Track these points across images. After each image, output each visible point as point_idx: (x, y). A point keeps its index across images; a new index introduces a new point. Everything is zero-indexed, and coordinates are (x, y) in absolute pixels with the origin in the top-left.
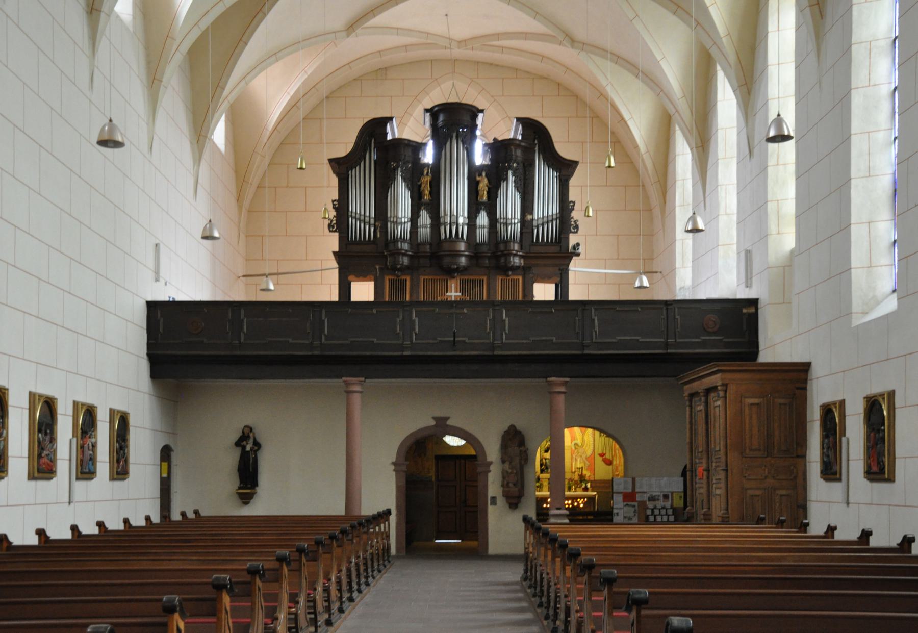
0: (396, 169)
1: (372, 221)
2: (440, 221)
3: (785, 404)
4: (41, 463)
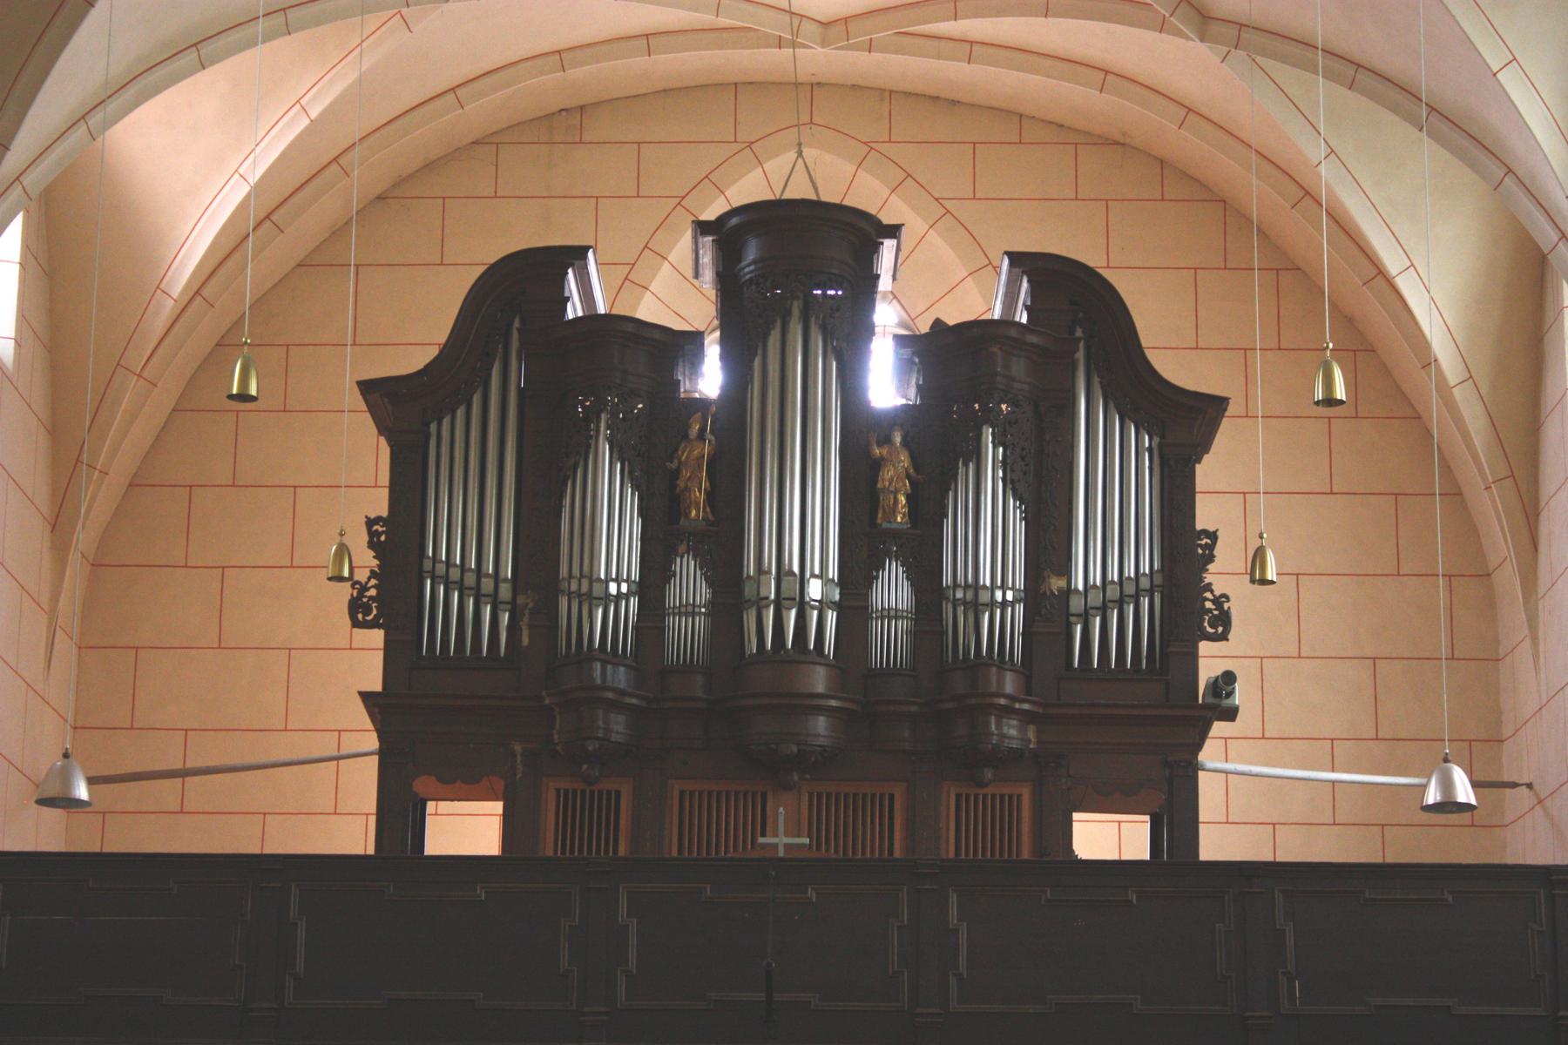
1: (505, 592)
2: (741, 592)
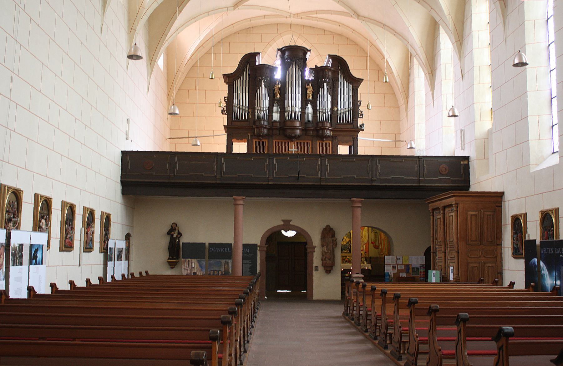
0: (261, 81)
1: (247, 109)
2: (285, 110)
3: (490, 215)
4: (66, 242)
